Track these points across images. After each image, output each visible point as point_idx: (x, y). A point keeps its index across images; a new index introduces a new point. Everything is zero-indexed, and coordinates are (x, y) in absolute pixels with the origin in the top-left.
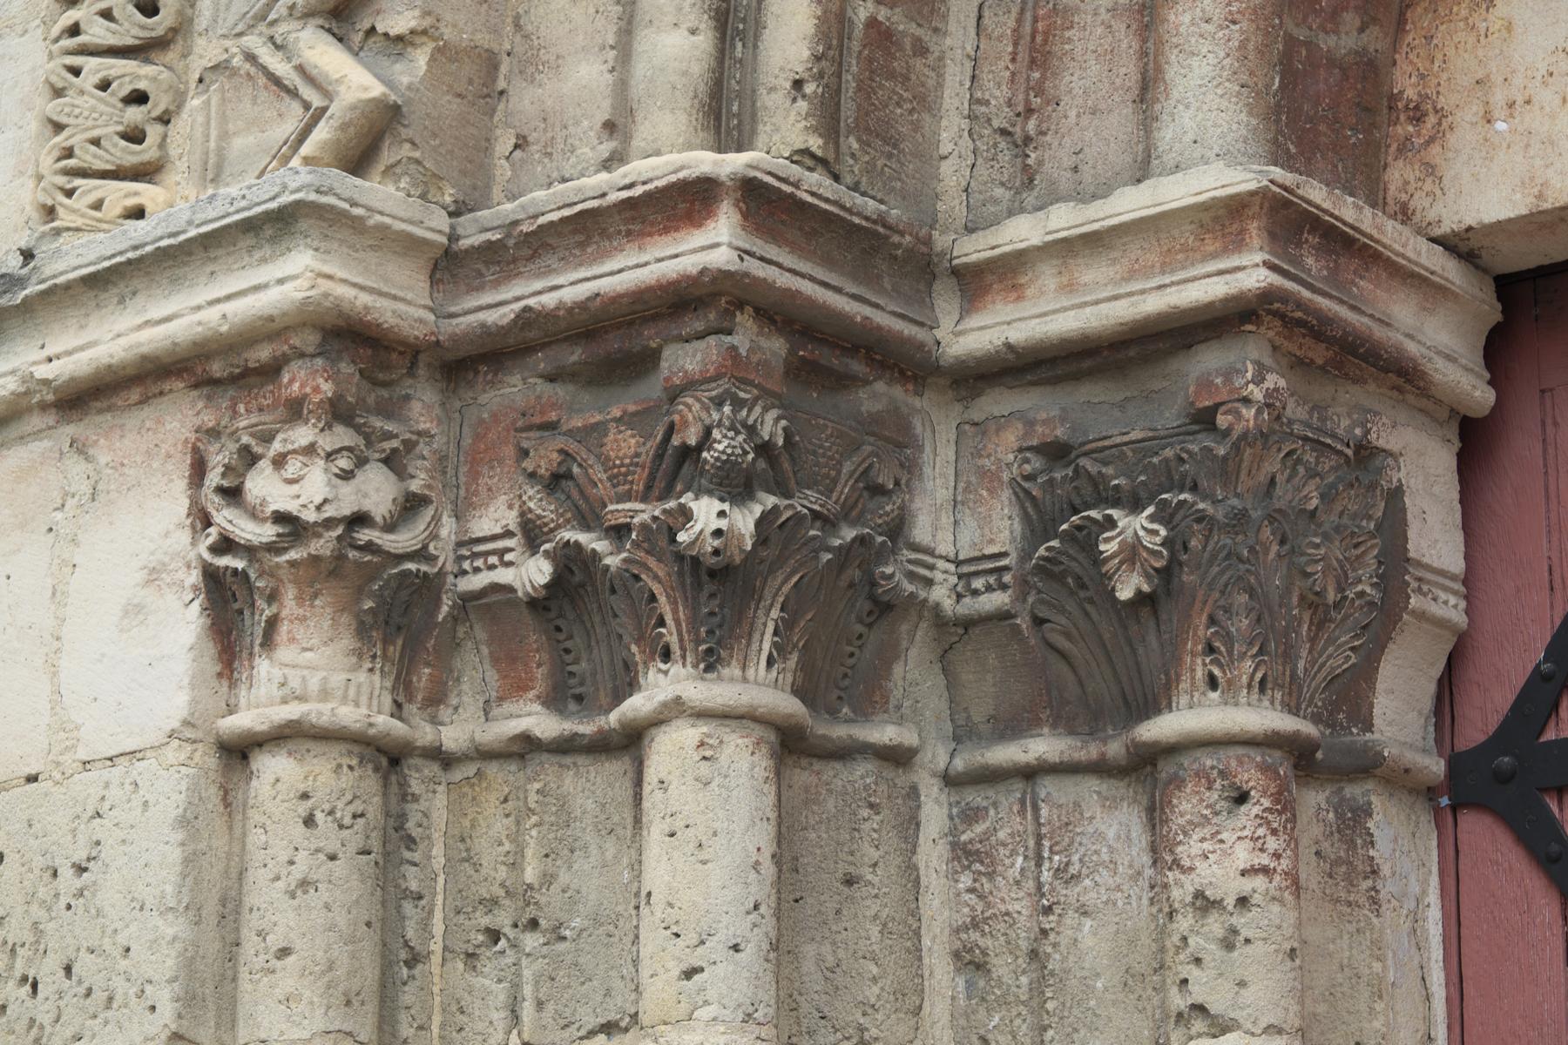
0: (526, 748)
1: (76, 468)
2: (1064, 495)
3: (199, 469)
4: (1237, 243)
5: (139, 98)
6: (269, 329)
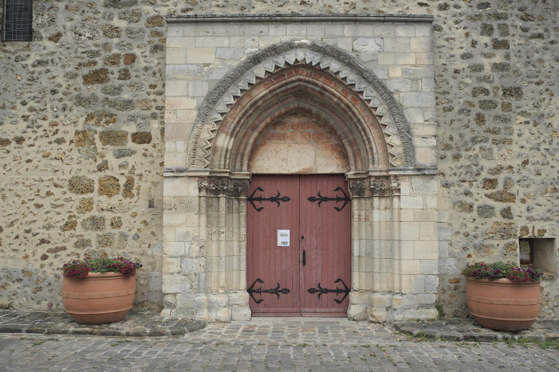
2: (236, 185)
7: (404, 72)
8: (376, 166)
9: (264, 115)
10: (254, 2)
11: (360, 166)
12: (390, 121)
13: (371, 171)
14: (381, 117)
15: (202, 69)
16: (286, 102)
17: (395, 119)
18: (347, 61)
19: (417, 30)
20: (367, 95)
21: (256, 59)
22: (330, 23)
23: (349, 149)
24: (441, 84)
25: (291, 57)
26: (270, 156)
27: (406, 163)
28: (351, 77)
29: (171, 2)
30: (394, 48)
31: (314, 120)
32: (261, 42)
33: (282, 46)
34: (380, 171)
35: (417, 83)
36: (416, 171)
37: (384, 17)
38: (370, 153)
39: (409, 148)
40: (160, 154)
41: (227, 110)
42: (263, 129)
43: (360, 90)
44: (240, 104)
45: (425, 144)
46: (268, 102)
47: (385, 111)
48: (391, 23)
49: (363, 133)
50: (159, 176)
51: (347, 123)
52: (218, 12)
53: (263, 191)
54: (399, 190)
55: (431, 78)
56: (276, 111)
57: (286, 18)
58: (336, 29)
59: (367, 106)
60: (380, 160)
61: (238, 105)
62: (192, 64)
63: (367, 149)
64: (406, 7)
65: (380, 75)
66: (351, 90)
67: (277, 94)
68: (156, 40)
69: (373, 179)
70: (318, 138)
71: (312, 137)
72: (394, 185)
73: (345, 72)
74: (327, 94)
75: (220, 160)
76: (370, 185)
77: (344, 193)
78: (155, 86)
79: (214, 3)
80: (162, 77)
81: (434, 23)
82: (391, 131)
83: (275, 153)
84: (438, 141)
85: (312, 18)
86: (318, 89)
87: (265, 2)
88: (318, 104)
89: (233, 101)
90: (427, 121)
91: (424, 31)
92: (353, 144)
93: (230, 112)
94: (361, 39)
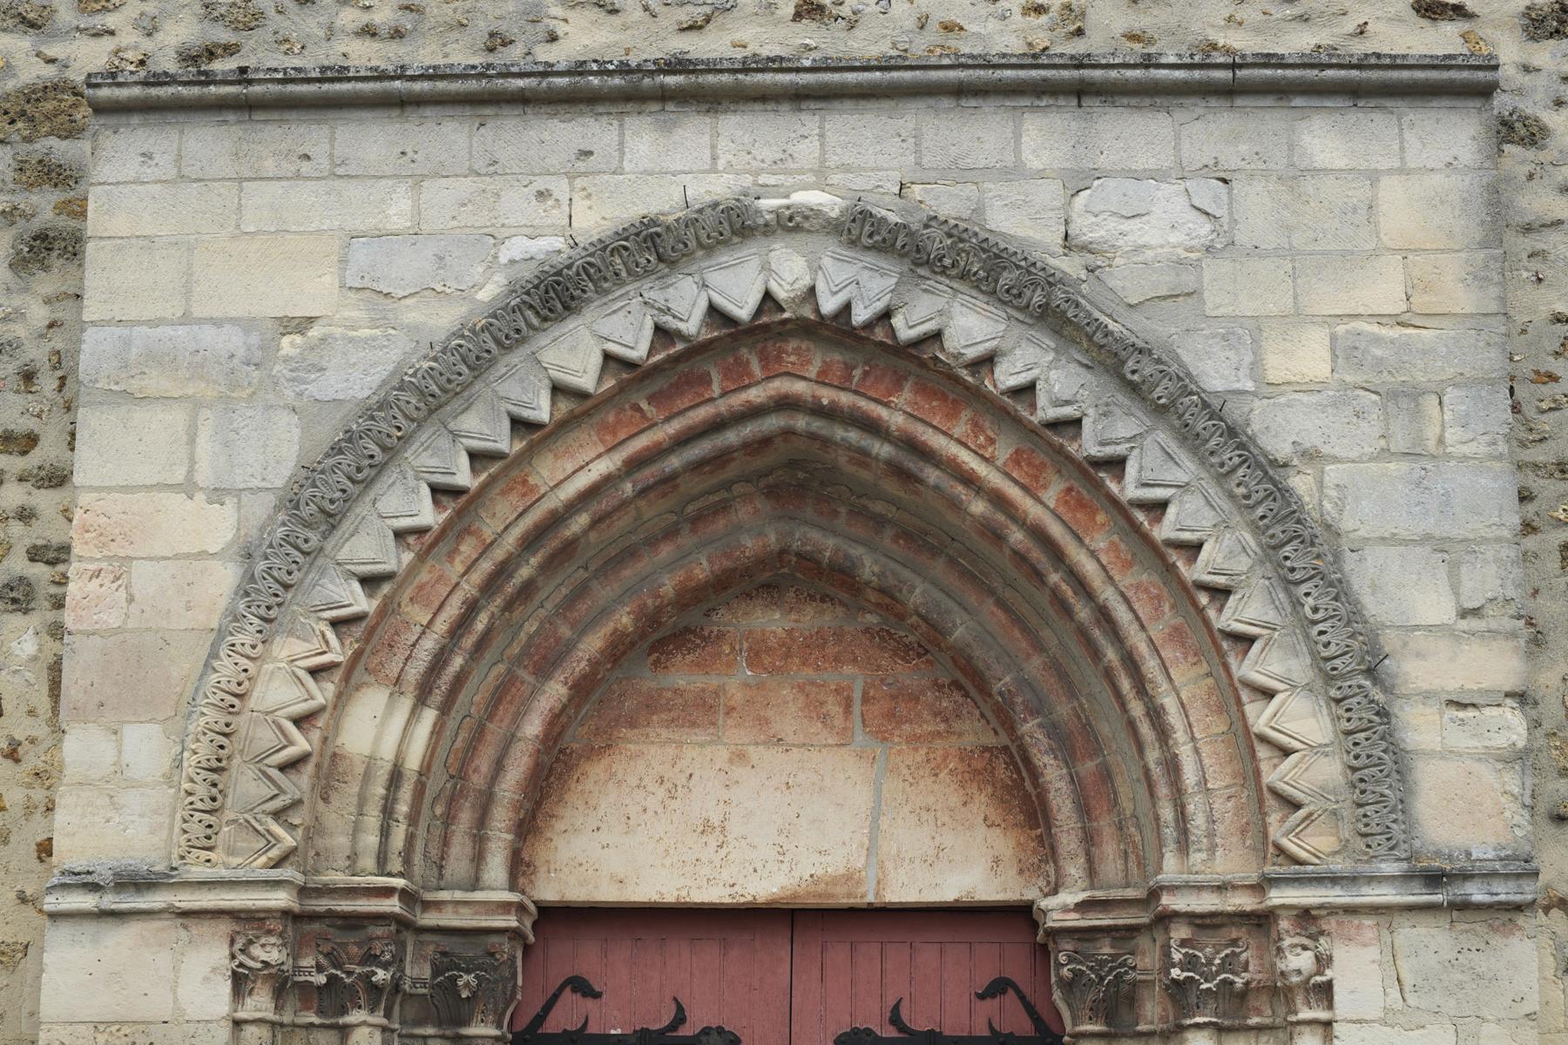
0: (312, 1025)
1: (183, 933)
2: (444, 965)
3: (232, 942)
4: (508, 913)
5: (210, 826)
6: (269, 911)
7: (1344, 352)
8: (1197, 858)
9: (603, 593)
10: (557, 11)
11: (1111, 867)
12: (1271, 616)
13: (1173, 889)
14: (1221, 593)
15: (269, 348)
16: (720, 524)
17: (1297, 604)
18: (1037, 298)
19: (1407, 135)
20: (1148, 476)
21: (555, 295)
22: (946, 103)
23: (1053, 773)
24: (1546, 423)
25: (738, 284)
26: (633, 810)
27: (1360, 844)
28: (1061, 383)
29: (131, 11)
30: (1289, 229)
31: (872, 619)
32: (580, 205)
33: (689, 223)
34: (1221, 888)
35: (1417, 414)
36: (1416, 886)
37: (1233, 66)
38: (1163, 790)
39: (1378, 762)
40: (39, 795)
41: (397, 560)
42: (594, 664)
43: (1109, 450)
44: (467, 531)
45: (1460, 740)
46: (622, 522)
47: (1242, 564)
48: (1268, 101)
49: (1126, 685)
50: (29, 911)
51: (1046, 633)
52: (363, 55)
53: (597, 996)
54: (1325, 992)
55: (1491, 383)
56: (671, 571)
57: (711, 79)
58: (981, 135)
59: (1146, 539)
60: (1220, 828)
61: (460, 537)
62: (217, 323)
63: (1147, 772)
64: (1350, 26)
65: (1216, 372)
66: (1060, 451)
67: (669, 480)
68: (44, 205)
69: (1180, 932)
70: (891, 715)
71: (857, 708)
72: (1299, 961)
73: (1027, 359)
74: (932, 475)
75: (356, 830)
76: (1168, 964)
77: (1030, 1009)
78: (31, 440)
79: (349, 18)
80: (68, 392)
81: (1502, 103)
82: (1276, 668)
83: (661, 792)
84: (1536, 724)
85: (851, 77)
86: (883, 450)
87: (614, 12)
88: (889, 533)
89: (427, 515)
90: (1476, 612)
91: (1448, 140)
92: (1074, 742)
93: (412, 570)
94: (1111, 183)
